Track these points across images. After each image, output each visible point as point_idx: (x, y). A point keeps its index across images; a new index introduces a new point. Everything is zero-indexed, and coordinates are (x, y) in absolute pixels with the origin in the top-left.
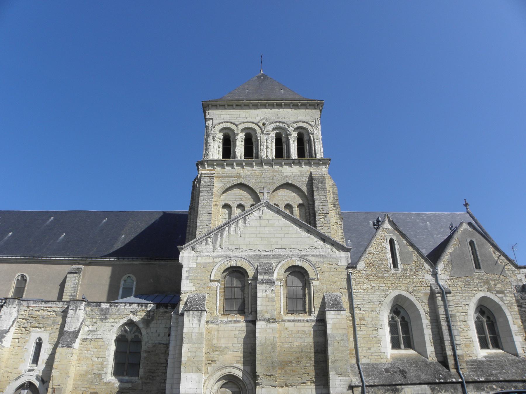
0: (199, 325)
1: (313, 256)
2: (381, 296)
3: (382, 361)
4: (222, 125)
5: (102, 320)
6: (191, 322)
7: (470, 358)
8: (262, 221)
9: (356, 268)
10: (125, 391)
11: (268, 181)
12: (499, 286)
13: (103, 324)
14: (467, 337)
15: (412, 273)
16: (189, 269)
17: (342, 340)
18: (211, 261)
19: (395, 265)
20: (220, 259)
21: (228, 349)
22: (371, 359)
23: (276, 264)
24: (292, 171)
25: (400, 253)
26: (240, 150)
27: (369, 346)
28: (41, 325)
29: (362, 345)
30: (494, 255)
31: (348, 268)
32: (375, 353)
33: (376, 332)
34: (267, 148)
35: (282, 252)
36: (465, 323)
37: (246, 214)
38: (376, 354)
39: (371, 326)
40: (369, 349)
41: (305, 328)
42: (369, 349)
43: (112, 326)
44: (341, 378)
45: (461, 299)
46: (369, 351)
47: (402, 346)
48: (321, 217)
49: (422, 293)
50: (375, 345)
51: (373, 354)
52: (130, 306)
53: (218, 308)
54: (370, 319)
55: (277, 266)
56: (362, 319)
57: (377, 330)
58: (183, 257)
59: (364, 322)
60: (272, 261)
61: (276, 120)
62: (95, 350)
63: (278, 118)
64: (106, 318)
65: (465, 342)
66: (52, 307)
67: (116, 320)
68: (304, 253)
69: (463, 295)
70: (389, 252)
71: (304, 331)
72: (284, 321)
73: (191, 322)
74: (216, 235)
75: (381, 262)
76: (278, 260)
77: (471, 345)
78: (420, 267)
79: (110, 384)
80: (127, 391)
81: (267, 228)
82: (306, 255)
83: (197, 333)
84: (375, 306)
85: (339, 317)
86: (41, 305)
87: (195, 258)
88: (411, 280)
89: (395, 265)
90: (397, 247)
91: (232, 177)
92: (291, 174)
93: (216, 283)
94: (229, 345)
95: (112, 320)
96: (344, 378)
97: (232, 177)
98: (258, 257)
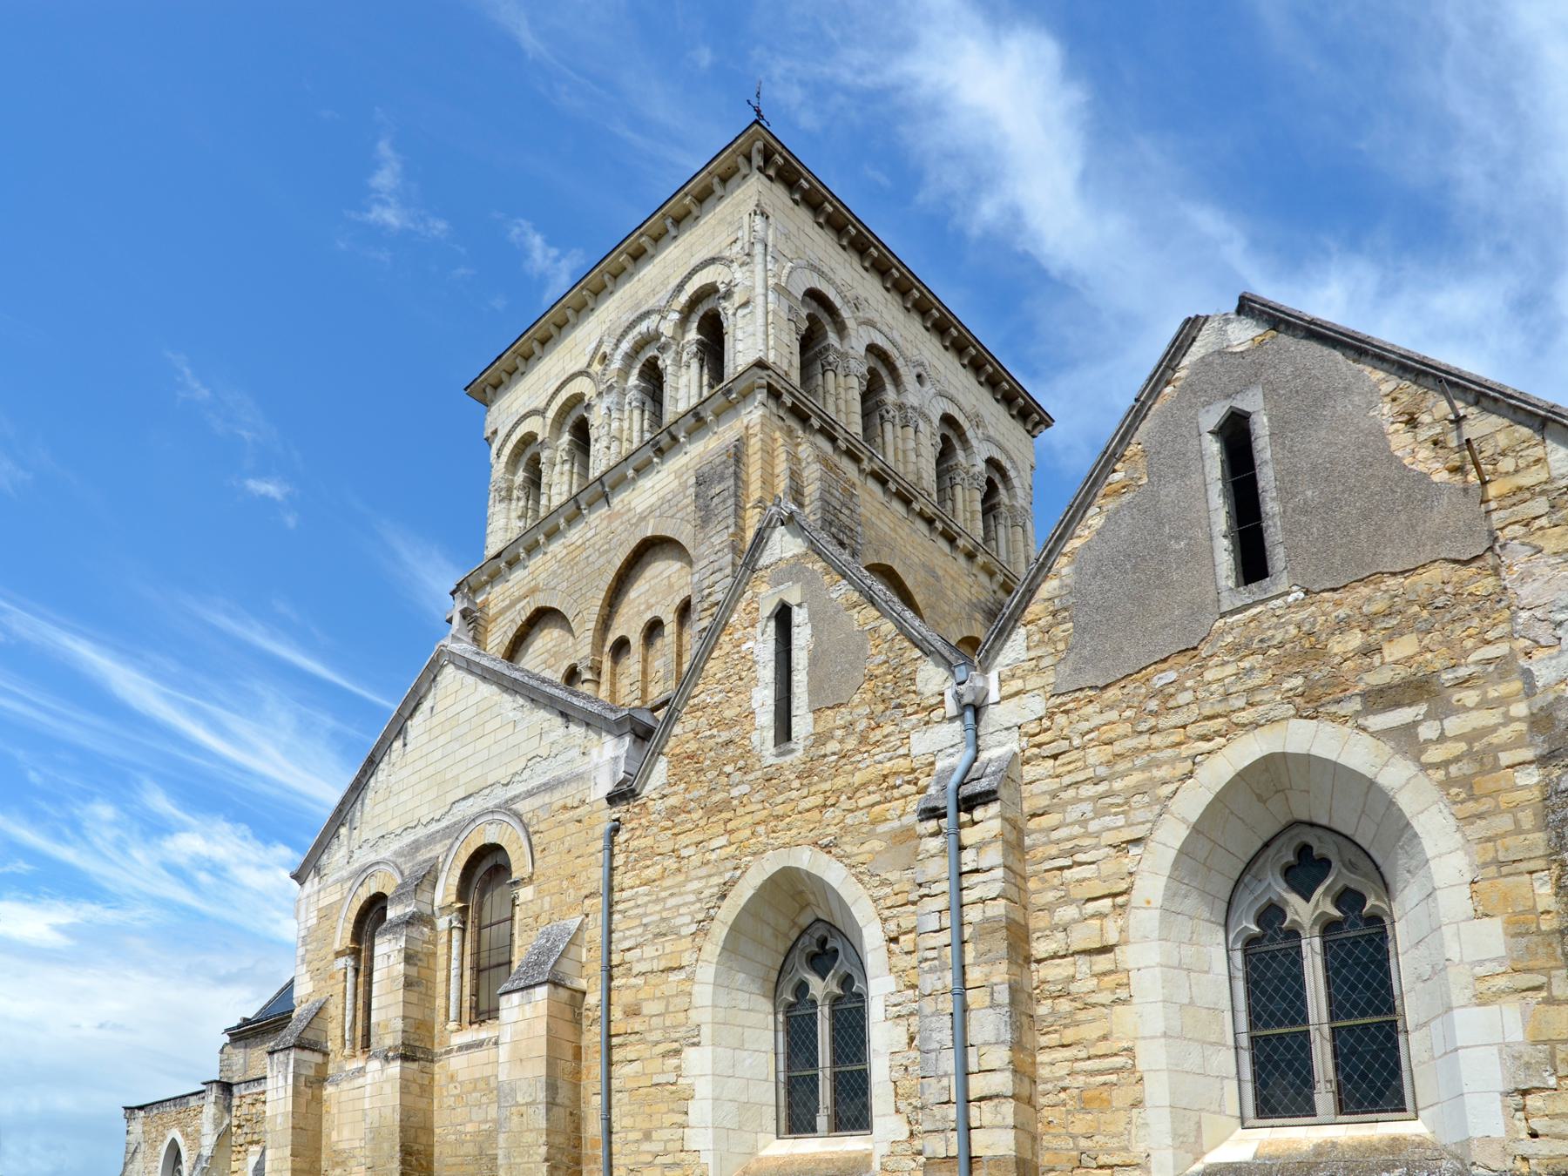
2: (707, 893)
12: (1406, 646)
14: (1102, 1048)
15: (851, 743)
19: (784, 731)
24: (658, 487)
25: (814, 661)
27: (646, 1125)
30: (1399, 440)
33: (674, 1062)
36: (1103, 962)
38: (668, 1159)
40: (647, 1136)
42: (647, 1136)
45: (1098, 814)
46: (646, 1146)
47: (1324, 1098)
49: (879, 837)
51: (659, 1160)
56: (633, 1012)
57: (677, 1052)
65: (1081, 1080)
69: (1118, 785)
77: (1120, 1097)
78: (897, 697)
82: (513, 799)
89: (784, 731)
90: (802, 637)
91: (519, 600)
97: (519, 600)
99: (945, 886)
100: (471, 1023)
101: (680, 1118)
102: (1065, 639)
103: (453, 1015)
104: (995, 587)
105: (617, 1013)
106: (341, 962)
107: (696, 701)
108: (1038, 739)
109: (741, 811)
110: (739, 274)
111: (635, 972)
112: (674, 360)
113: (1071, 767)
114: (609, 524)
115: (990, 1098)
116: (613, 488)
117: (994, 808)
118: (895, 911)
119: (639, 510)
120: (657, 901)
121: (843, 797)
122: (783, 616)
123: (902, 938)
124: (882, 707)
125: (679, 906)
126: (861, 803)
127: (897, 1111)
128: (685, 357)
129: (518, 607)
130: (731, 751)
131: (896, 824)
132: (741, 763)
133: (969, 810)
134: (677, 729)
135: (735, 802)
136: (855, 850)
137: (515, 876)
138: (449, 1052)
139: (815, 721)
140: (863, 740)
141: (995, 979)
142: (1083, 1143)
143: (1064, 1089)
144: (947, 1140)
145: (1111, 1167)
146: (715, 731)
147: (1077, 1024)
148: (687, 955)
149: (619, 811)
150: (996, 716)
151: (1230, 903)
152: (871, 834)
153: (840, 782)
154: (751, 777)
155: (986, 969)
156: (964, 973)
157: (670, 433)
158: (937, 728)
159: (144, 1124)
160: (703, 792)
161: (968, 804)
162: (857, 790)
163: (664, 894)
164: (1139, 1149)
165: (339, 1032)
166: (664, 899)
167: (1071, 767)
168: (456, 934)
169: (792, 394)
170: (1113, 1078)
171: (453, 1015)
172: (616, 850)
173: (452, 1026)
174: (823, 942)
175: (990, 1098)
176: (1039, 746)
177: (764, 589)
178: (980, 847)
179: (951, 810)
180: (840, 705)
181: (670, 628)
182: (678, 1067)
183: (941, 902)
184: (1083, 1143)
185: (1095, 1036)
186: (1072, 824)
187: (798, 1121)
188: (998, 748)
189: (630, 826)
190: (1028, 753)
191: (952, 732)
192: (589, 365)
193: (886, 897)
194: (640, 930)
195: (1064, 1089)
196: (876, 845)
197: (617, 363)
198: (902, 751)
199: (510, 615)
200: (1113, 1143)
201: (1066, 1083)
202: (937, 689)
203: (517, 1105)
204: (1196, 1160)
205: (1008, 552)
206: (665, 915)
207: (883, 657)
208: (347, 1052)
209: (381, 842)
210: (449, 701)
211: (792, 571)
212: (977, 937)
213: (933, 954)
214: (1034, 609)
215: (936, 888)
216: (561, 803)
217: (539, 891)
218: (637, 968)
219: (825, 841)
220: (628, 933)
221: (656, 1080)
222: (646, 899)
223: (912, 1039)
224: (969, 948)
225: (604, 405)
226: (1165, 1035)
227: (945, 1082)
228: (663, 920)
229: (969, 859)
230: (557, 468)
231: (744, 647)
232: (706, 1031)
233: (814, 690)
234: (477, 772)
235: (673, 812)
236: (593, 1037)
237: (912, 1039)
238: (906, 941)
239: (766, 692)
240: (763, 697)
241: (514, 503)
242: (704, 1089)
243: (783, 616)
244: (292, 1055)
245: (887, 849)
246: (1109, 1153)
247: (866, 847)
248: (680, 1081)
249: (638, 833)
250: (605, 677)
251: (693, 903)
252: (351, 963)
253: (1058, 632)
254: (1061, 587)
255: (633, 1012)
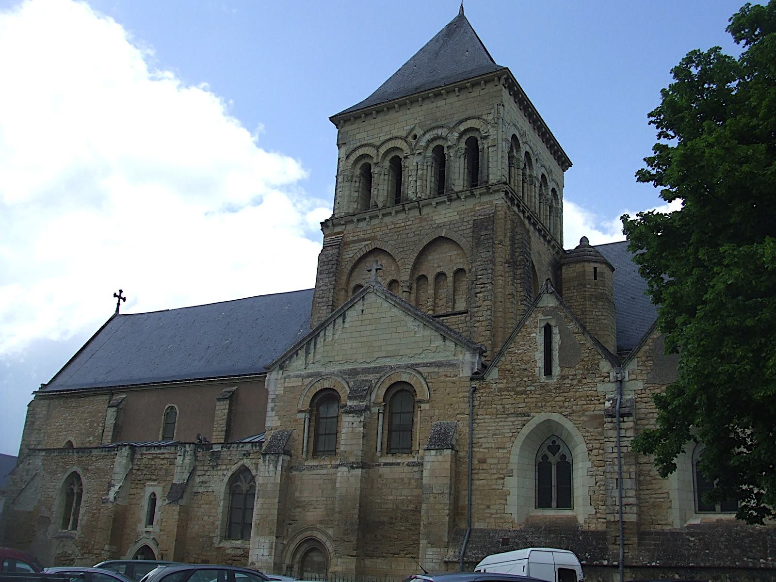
0: (275, 473)
1: (426, 365)
3: (506, 526)
4: (357, 152)
5: (213, 467)
6: (266, 470)
7: (659, 528)
8: (365, 317)
9: (483, 379)
10: (236, 558)
11: (413, 239)
13: (215, 473)
14: (660, 491)
16: (275, 396)
17: (441, 494)
18: (300, 384)
19: (548, 372)
20: (310, 379)
21: (311, 504)
22: (489, 523)
23: (376, 381)
24: (448, 215)
25: (560, 349)
26: (382, 189)
27: (488, 503)
28: (154, 477)
29: (480, 501)
31: (472, 379)
32: (497, 513)
33: (502, 481)
34: (417, 179)
35: (388, 362)
37: (345, 309)
38: (498, 516)
39: (494, 471)
40: (488, 507)
41: (403, 476)
42: (488, 507)
43: (223, 474)
44: (434, 549)
46: (487, 511)
48: (478, 291)
50: (497, 502)
52: (242, 447)
53: (304, 449)
54: (495, 461)
55: (377, 383)
56: (483, 461)
58: (269, 380)
59: (485, 466)
60: (371, 377)
61: (433, 125)
62: (207, 506)
63: (436, 120)
64: (217, 465)
66: (164, 454)
67: (228, 467)
68: (413, 361)
70: (541, 348)
71: (402, 479)
72: (379, 465)
73: (266, 470)
74: (308, 344)
75: (523, 367)
76: (378, 375)
78: (592, 369)
79: (222, 549)
80: (238, 558)
81: (369, 327)
82: (416, 364)
83: (273, 484)
84: (506, 440)
85: (440, 458)
86: (153, 452)
87: (282, 381)
88: (571, 394)
89: (548, 372)
90: (556, 339)
91: (365, 240)
92: (446, 220)
93: (304, 414)
94: (312, 499)
95: (224, 467)
96: (439, 550)
97: (365, 240)
98: (354, 373)
99: (615, 440)
100: (387, 453)
101: (503, 502)
102: (650, 366)
103: (379, 449)
104: (554, 253)
105: (475, 462)
106: (302, 415)
107: (510, 350)
108: (640, 396)
109: (530, 396)
110: (492, 132)
111: (484, 446)
112: (454, 154)
113: (651, 407)
114: (420, 222)
115: (629, 505)
116: (423, 206)
117: (631, 418)
118: (592, 441)
119: (437, 222)
120: (494, 422)
121: (572, 400)
122: (548, 330)
123: (593, 451)
124: (586, 372)
125: (504, 426)
126: (579, 403)
127: (591, 505)
128: (459, 154)
129: (364, 243)
130: (526, 373)
131: (592, 413)
132: (530, 378)
133: (623, 417)
134: (503, 359)
135: (528, 392)
136: (577, 419)
137: (418, 398)
138: (379, 465)
139: (561, 371)
140: (580, 381)
141: (631, 470)
142: (654, 518)
143: (648, 502)
144: (614, 516)
145: (661, 524)
146: (519, 364)
147: (652, 484)
148: (508, 444)
149: (475, 384)
150: (629, 385)
151: (693, 452)
152: (583, 415)
153: (571, 394)
154: (535, 384)
155: (628, 467)
156: (621, 467)
157: (457, 195)
158: (606, 384)
159: (44, 460)
160: (515, 385)
161: (623, 415)
162: (578, 398)
163: (497, 420)
164: (670, 520)
165: (301, 447)
166: (498, 422)
167: (651, 407)
168: (381, 416)
169: (511, 193)
170: (663, 500)
171: (379, 449)
172: (475, 399)
173: (379, 454)
174: (554, 442)
175: (629, 505)
176: (641, 398)
177: (541, 316)
178: (626, 429)
179: (617, 415)
180: (571, 367)
181: (450, 279)
182: (504, 484)
183: (613, 444)
184: (654, 518)
185: (657, 488)
186: (652, 425)
187: (543, 502)
188: (629, 396)
189: (481, 391)
190: (637, 400)
191: (612, 386)
192: (407, 137)
193: (588, 436)
194: (486, 432)
195: (648, 502)
196: (585, 418)
197: (423, 143)
198: (595, 389)
199: (358, 246)
200: (663, 518)
201: (648, 500)
202: (607, 371)
203: (433, 493)
204: (685, 523)
205: (554, 230)
206: (498, 428)
207: (587, 355)
208: (304, 456)
209: (329, 364)
210: (373, 311)
211: (552, 312)
212: (625, 457)
213: (611, 460)
214: (640, 354)
215: (611, 440)
216: (444, 373)
217: (432, 407)
218: (484, 446)
219: (565, 413)
220: (480, 432)
221: (493, 487)
222: (489, 420)
223: (596, 483)
224: (622, 460)
225: (415, 161)
226: (678, 489)
227: (614, 499)
228: (497, 429)
229: (623, 433)
230: (382, 176)
231: (532, 335)
232: (515, 472)
233: (561, 359)
234: (394, 348)
235: (500, 390)
236: (464, 468)
237: (596, 483)
238: (595, 452)
239: (541, 354)
240: (540, 356)
241: (353, 183)
242: (514, 492)
243: (548, 330)
244: (281, 458)
245: (589, 421)
246: (662, 520)
247: (581, 418)
248: (504, 488)
249: (485, 394)
250: (414, 291)
251: (510, 426)
252: (308, 416)
253: (648, 363)
254: (650, 349)
255: (483, 461)
